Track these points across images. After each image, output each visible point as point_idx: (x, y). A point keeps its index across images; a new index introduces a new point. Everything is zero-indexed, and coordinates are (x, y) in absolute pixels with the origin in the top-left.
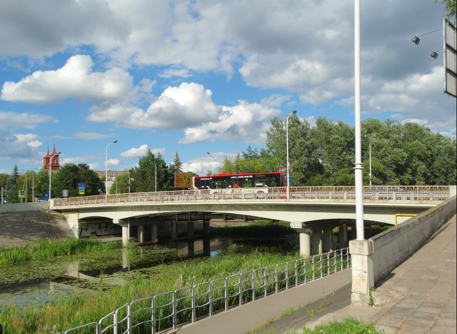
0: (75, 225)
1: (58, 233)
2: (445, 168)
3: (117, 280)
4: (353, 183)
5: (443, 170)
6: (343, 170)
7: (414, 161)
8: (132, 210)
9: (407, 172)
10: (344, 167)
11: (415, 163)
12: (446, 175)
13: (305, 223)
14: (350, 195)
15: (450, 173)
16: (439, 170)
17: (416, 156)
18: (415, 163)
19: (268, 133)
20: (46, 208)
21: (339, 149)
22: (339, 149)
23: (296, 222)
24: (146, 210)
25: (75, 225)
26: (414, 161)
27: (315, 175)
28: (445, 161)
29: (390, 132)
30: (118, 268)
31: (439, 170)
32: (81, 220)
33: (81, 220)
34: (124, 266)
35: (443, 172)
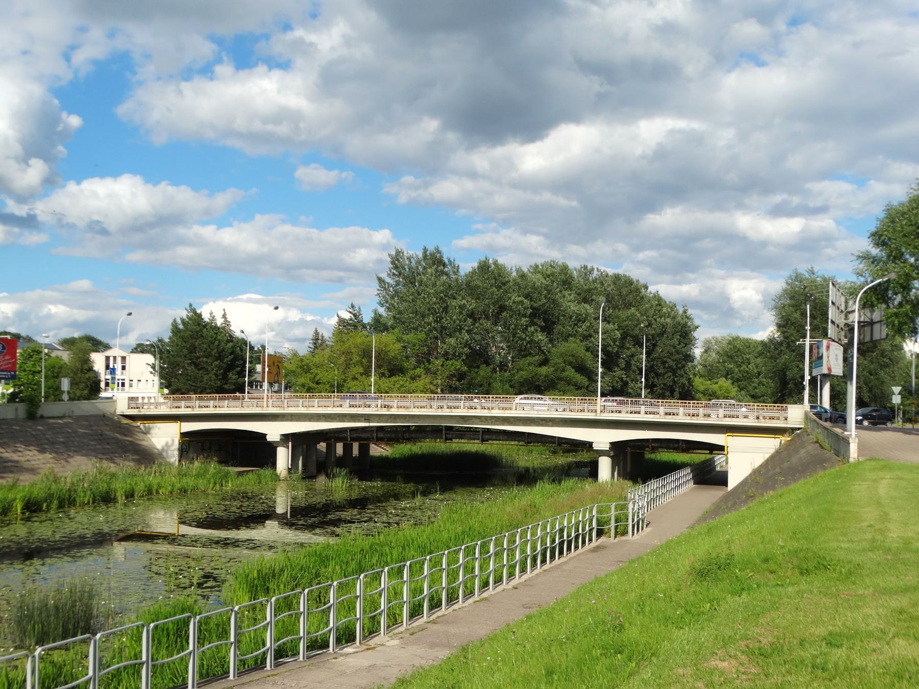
0: (173, 441)
1: (147, 457)
2: (673, 360)
3: (270, 531)
4: (803, 400)
5: (671, 363)
6: (530, 359)
7: (628, 345)
8: (326, 421)
9: (618, 366)
10: (530, 354)
11: (628, 349)
12: (674, 372)
13: (611, 443)
14: (591, 408)
15: (680, 368)
16: (664, 363)
17: (631, 336)
18: (628, 349)
19: (380, 280)
20: (112, 411)
21: (524, 321)
22: (524, 321)
23: (601, 443)
24: (359, 421)
25: (173, 441)
26: (628, 345)
27: (478, 367)
28: (675, 347)
29: (589, 291)
30: (267, 515)
31: (664, 363)
32: (183, 435)
33: (183, 435)
34: (280, 510)
35: (670, 367)
